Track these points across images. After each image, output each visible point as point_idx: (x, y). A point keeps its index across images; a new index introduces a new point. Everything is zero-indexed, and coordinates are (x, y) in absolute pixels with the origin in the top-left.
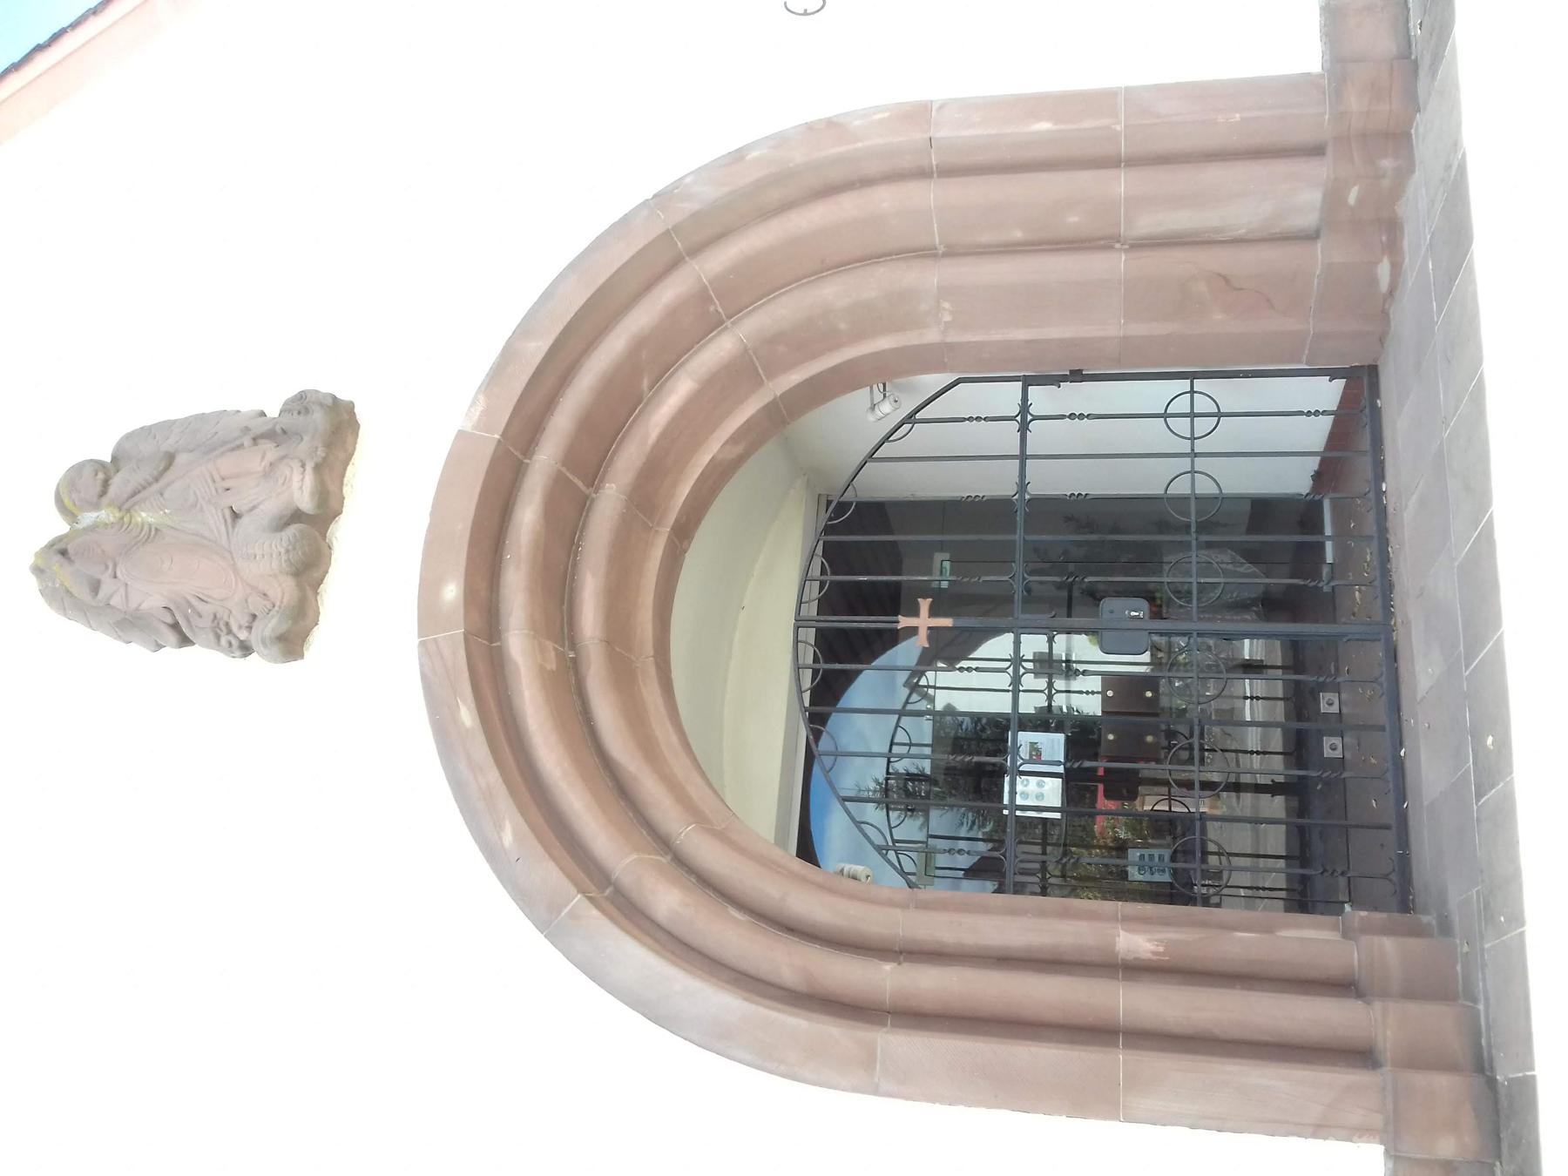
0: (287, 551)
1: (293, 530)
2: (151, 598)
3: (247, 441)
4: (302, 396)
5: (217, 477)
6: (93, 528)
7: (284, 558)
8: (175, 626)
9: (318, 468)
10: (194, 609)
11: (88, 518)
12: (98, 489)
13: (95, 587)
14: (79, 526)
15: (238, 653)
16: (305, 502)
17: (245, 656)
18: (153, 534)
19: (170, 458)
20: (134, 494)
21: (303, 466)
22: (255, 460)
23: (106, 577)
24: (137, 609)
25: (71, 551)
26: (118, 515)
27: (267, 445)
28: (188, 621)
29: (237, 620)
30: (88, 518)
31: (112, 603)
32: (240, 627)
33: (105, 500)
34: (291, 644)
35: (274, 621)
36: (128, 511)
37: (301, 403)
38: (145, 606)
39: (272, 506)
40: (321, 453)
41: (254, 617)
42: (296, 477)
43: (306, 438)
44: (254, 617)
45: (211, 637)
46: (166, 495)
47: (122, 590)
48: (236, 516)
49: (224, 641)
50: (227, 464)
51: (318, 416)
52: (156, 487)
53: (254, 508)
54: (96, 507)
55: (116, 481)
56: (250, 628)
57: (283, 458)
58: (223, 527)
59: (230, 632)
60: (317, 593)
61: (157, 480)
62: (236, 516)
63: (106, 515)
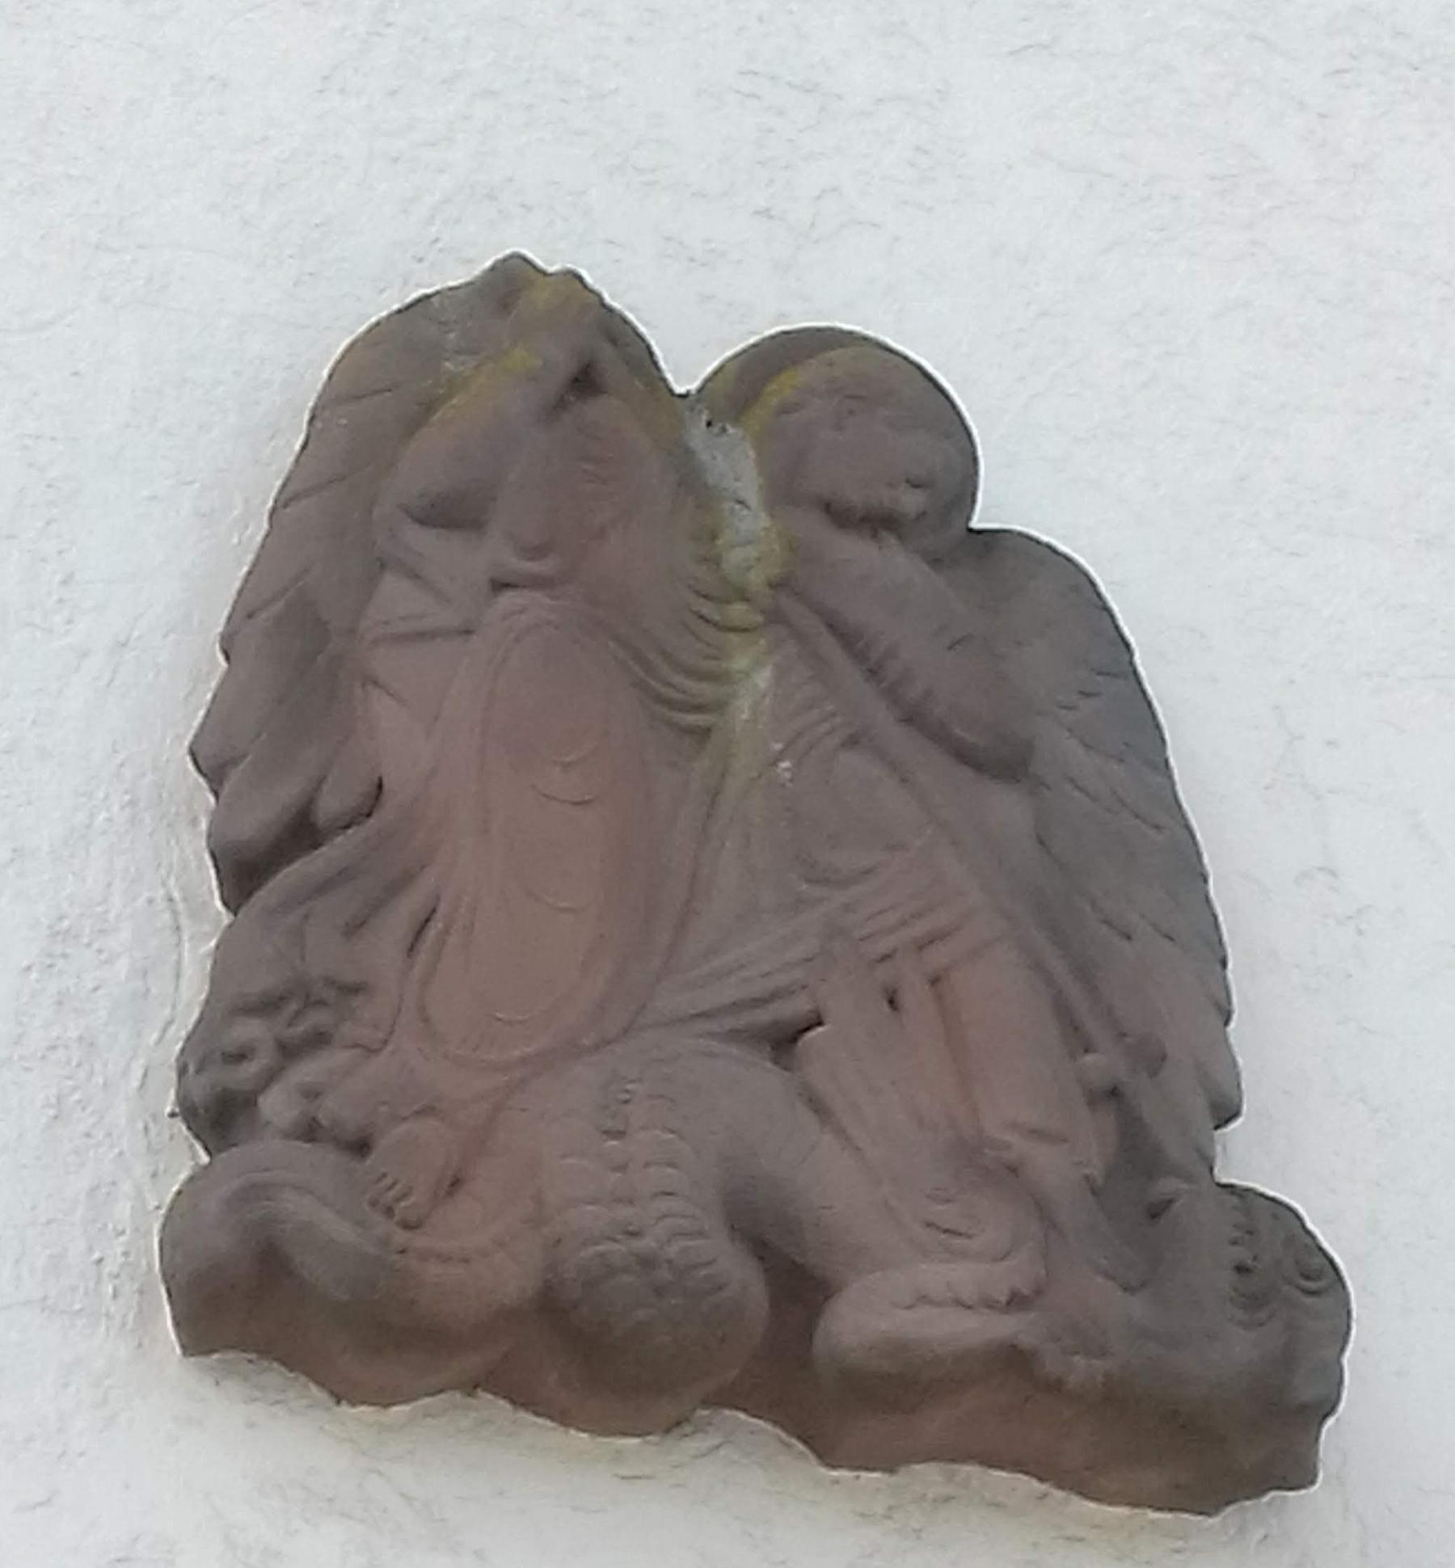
0: (647, 1262)
1: (740, 1275)
2: (414, 729)
3: (1102, 1064)
4: (1318, 1277)
5: (938, 956)
6: (692, 485)
7: (617, 1249)
8: (302, 832)
9: (1013, 1360)
10: (376, 906)
11: (735, 464)
12: (855, 496)
13: (453, 513)
14: (697, 435)
15: (201, 1088)
16: (866, 1318)
17: (188, 1111)
18: (687, 722)
19: (1005, 762)
20: (848, 638)
21: (1016, 1302)
22: (1024, 1099)
23: (493, 551)
24: (371, 681)
25: (595, 409)
26: (756, 579)
27: (1091, 1145)
28: (323, 887)
29: (340, 1079)
30: (735, 464)
31: (392, 585)
32: (312, 1094)
33: (813, 527)
34: (262, 1300)
35: (342, 1231)
36: (775, 617)
37: (1290, 1282)
38: (382, 706)
39: (834, 1184)
40: (1081, 1369)
41: (361, 1147)
42: (964, 1276)
43: (1137, 1307)
44: (361, 1147)
45: (262, 982)
46: (850, 761)
47: (447, 618)
48: (784, 1042)
49: (252, 1030)
50: (999, 989)
51: (1235, 1349)
52: (882, 717)
53: (818, 1107)
54: (784, 492)
55: (893, 563)
56: (310, 1131)
57: (1042, 1209)
58: (729, 992)
59: (289, 1052)
60: (472, 1387)
61: (912, 718)
62: (784, 1042)
63: (751, 534)
